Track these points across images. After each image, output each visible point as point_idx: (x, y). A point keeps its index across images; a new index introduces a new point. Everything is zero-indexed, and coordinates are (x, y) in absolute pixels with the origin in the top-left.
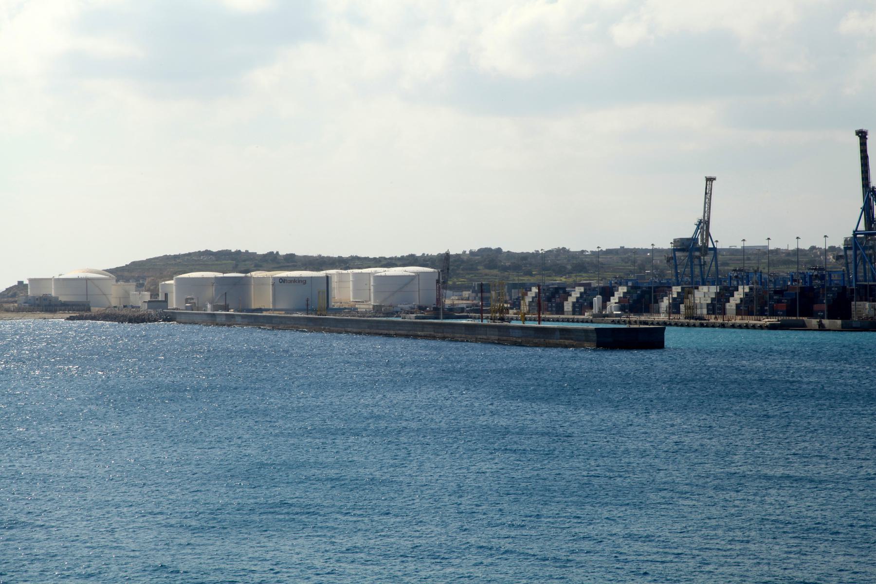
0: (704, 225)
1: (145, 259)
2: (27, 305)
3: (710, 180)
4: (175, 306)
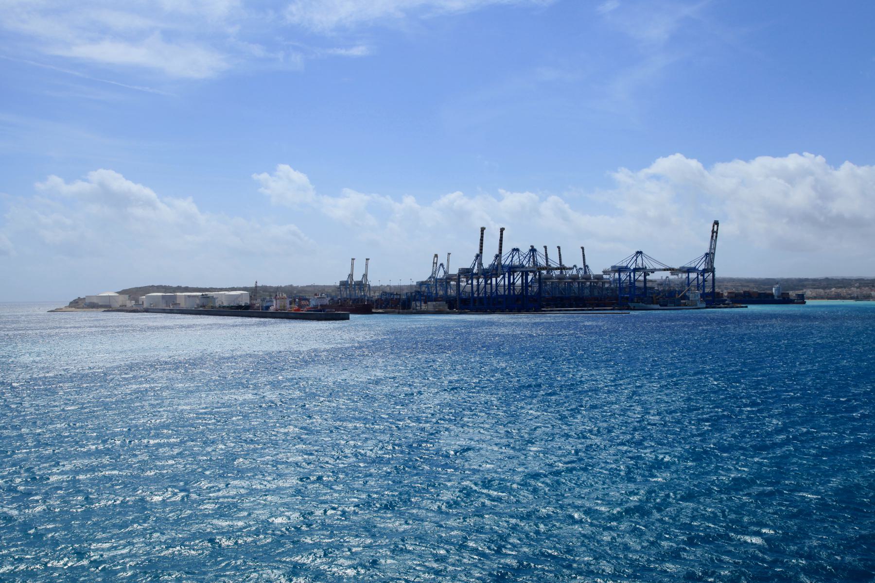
0: (710, 256)
3: (449, 254)
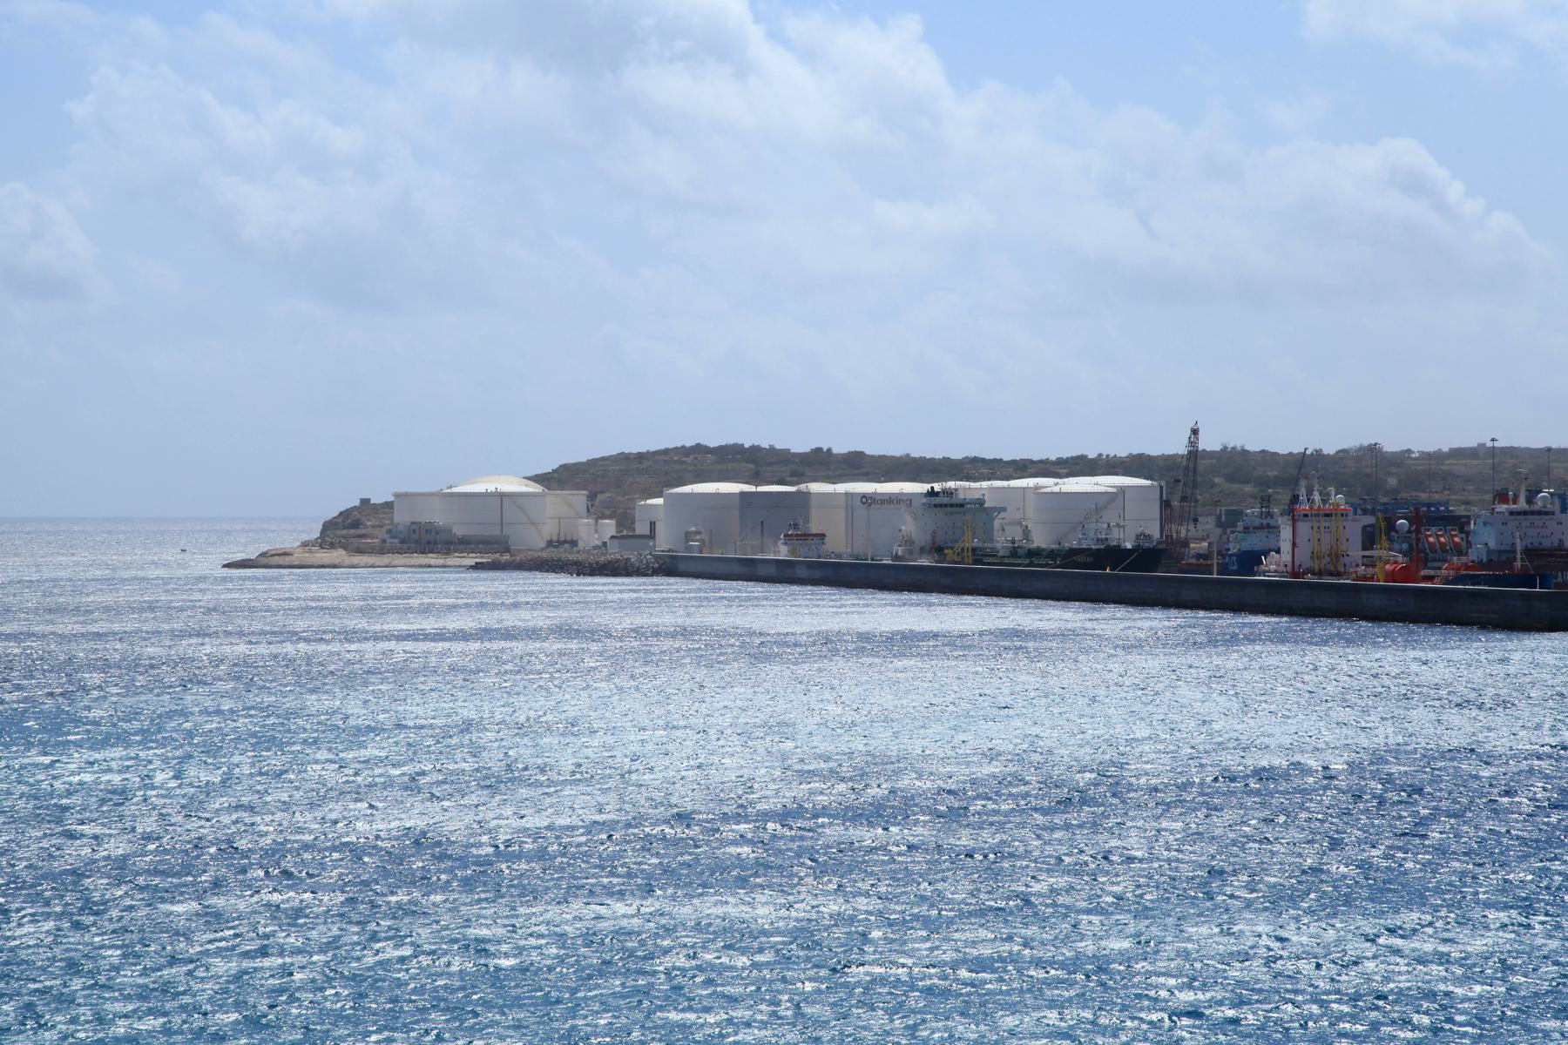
1: (584, 460)
2: (396, 541)
4: (666, 547)
